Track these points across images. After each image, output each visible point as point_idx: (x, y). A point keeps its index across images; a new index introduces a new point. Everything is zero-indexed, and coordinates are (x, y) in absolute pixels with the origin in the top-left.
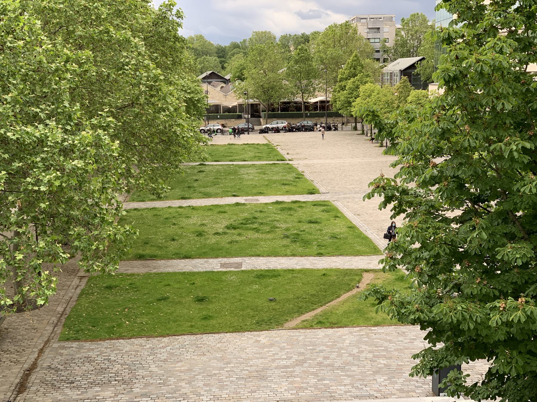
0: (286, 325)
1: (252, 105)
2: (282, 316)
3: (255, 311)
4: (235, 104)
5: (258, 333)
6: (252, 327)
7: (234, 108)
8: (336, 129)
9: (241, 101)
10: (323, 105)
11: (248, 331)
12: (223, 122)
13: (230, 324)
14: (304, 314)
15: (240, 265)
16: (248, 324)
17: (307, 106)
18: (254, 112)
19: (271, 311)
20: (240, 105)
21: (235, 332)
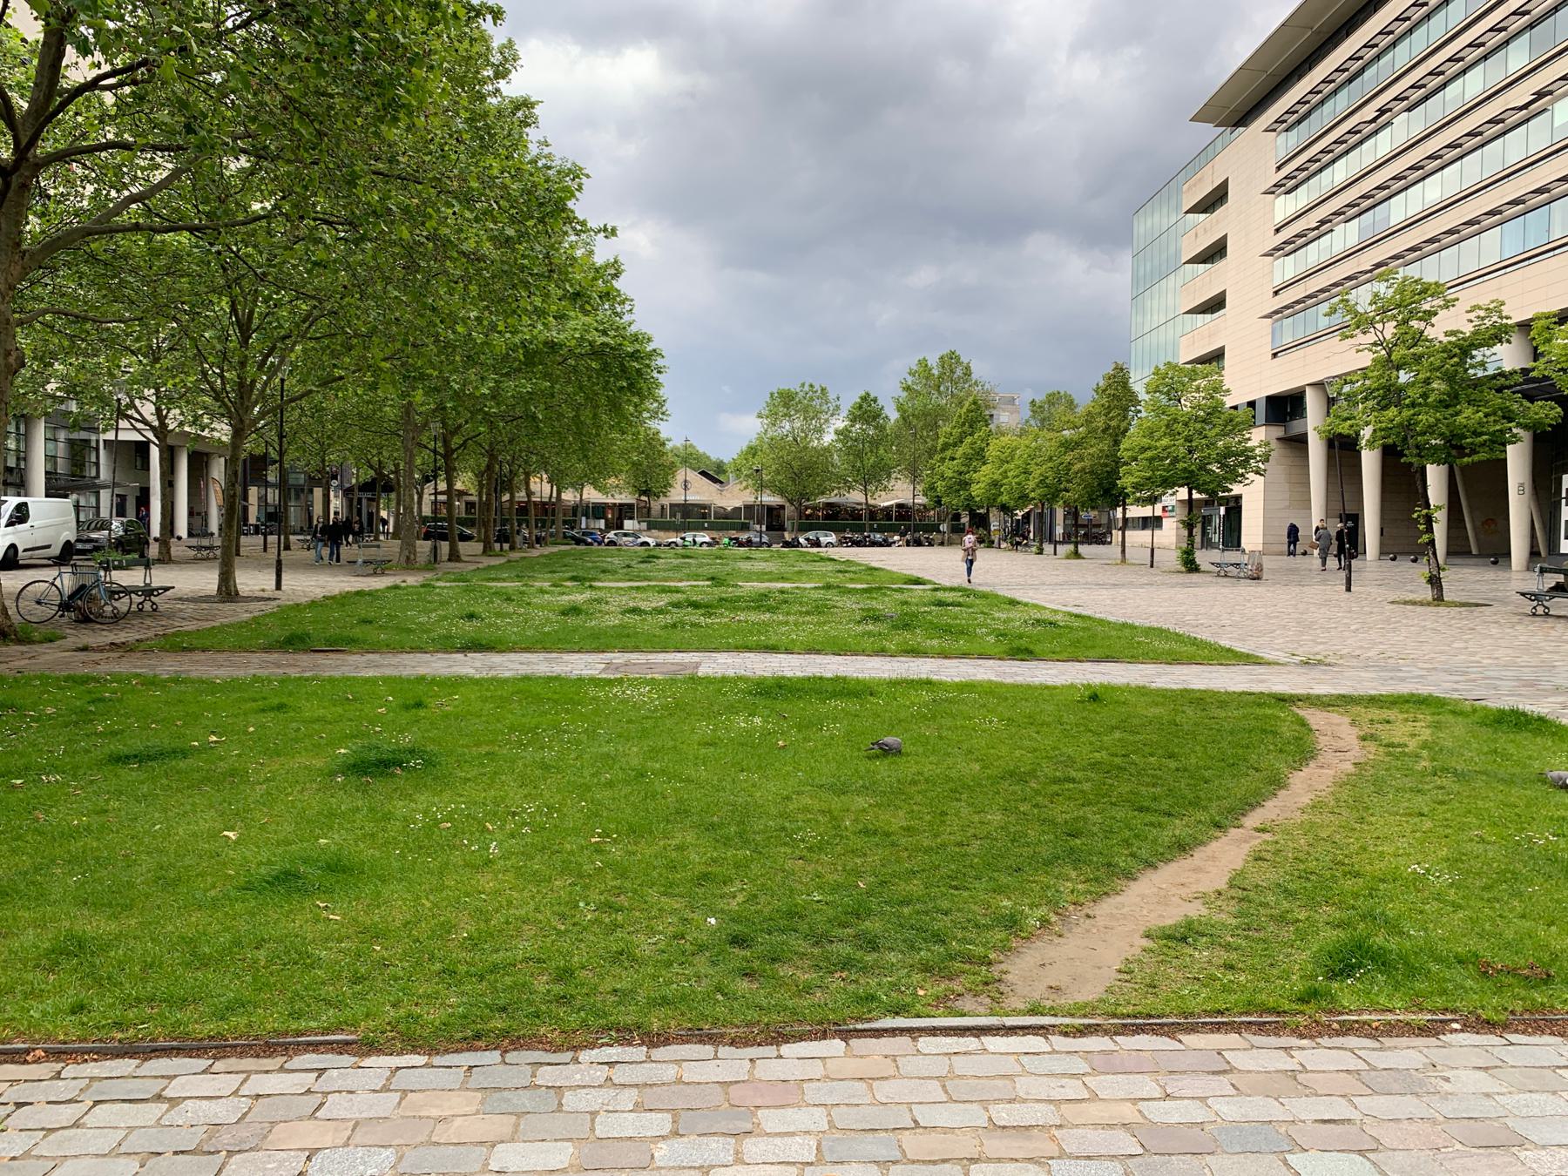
0: (1029, 970)
1: (770, 509)
2: (956, 882)
3: (727, 842)
4: (738, 504)
5: (731, 1063)
6: (679, 981)
7: (737, 510)
8: (931, 545)
9: (750, 499)
10: (903, 511)
11: (624, 1035)
12: (715, 534)
13: (473, 943)
14: (1130, 876)
15: (697, 665)
16: (645, 945)
17: (873, 513)
18: (773, 519)
19: (857, 842)
20: (749, 508)
21: (473, 1041)
